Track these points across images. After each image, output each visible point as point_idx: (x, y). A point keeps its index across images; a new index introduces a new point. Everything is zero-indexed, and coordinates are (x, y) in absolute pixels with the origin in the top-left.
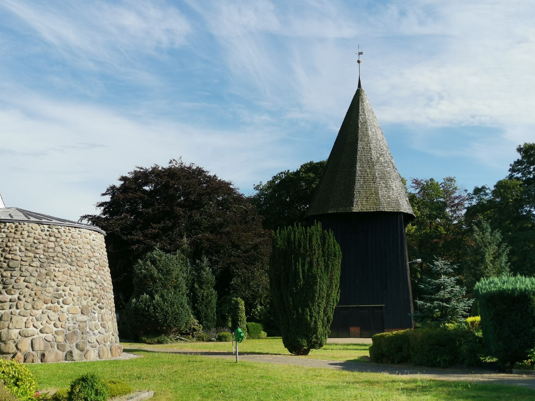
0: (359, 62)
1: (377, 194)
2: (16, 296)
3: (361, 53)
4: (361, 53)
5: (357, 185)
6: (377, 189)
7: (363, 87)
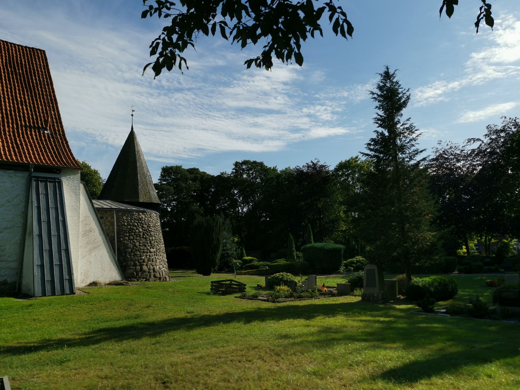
0: (132, 115)
1: (150, 193)
2: (155, 249)
3: (133, 111)
4: (133, 111)
5: (140, 187)
6: (149, 189)
7: (134, 130)
